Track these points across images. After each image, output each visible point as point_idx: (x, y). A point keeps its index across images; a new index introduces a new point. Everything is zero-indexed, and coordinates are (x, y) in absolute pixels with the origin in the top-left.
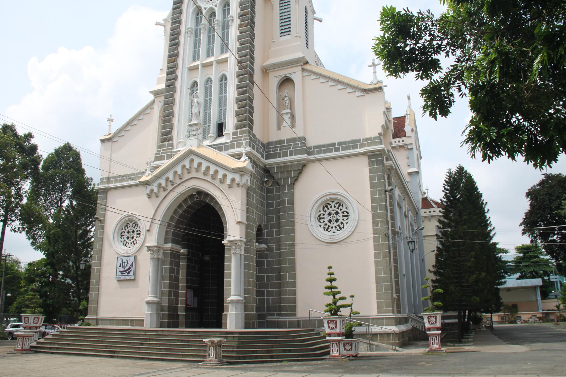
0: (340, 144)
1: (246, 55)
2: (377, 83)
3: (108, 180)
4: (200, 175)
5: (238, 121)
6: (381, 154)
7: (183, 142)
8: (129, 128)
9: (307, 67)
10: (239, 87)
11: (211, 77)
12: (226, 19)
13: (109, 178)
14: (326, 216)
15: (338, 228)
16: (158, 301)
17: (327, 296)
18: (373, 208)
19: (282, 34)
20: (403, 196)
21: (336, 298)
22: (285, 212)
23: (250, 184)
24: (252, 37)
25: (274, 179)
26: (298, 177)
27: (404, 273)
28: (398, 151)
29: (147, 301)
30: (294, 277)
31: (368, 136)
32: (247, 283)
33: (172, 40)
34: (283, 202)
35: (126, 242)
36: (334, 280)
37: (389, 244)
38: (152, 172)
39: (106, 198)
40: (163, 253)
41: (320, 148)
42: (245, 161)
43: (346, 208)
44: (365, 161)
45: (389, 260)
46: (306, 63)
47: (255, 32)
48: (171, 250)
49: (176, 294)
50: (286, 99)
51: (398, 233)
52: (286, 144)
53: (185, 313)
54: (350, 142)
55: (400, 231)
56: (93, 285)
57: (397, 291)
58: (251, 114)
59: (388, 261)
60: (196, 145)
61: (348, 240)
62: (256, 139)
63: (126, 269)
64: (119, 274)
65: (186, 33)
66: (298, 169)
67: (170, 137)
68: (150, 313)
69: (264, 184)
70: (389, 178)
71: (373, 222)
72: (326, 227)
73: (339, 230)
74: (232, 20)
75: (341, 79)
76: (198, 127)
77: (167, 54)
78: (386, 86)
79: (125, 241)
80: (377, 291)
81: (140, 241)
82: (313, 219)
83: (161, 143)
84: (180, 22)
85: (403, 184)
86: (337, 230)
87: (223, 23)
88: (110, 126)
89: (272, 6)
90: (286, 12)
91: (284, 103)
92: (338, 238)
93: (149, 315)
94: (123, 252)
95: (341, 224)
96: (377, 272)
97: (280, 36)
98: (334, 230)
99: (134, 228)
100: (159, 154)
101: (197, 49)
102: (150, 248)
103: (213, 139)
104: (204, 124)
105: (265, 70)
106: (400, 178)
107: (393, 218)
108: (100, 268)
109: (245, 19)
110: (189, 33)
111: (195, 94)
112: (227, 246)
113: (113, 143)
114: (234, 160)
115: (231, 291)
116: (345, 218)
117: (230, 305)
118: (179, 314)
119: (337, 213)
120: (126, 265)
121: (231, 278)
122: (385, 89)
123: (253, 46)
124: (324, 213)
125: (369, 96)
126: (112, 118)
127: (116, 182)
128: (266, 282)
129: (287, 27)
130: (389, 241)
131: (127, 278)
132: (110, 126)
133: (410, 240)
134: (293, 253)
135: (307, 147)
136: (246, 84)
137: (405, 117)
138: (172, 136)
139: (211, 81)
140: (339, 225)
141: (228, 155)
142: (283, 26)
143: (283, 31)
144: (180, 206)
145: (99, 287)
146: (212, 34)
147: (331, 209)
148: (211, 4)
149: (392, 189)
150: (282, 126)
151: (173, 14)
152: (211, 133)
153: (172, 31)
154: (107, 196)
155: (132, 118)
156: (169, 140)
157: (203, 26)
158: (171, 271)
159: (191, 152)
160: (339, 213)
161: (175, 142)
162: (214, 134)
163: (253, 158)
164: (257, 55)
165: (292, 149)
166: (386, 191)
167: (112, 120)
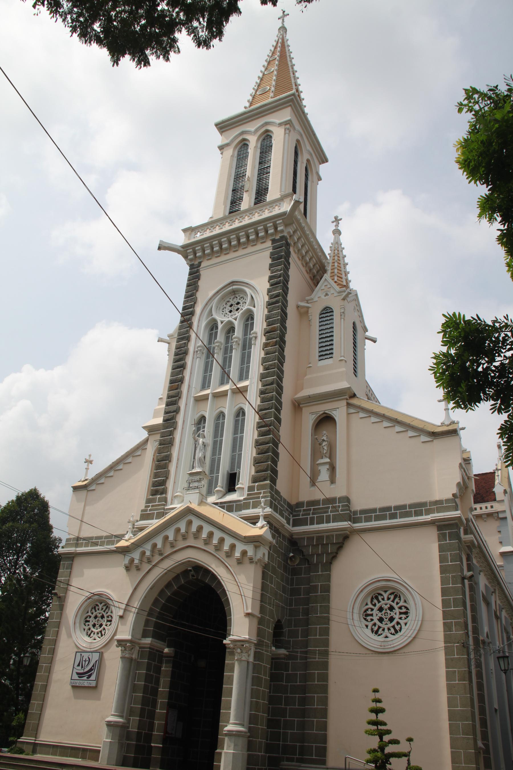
0: (397, 508)
1: (272, 383)
2: (450, 424)
3: (77, 541)
4: (200, 544)
5: (257, 472)
6: (456, 524)
7: (180, 496)
8: (111, 474)
9: (354, 401)
10: (259, 426)
11: (224, 411)
12: (248, 337)
13: (78, 539)
14: (375, 612)
15: (392, 631)
16: (124, 723)
17: (370, 736)
18: (445, 603)
19: (322, 358)
20: (492, 586)
21: (384, 740)
23: (269, 559)
24: (281, 359)
25: (303, 555)
26: (337, 553)
27: (496, 706)
28: (485, 521)
29: (107, 722)
30: (325, 701)
31: (437, 498)
32: (254, 706)
33: (175, 361)
34: (314, 589)
35: (90, 631)
36: (382, 711)
37: (469, 660)
38: (134, 535)
39: (71, 567)
40: (139, 651)
42: (262, 527)
43: (405, 601)
44: (433, 533)
45: (470, 684)
46: (352, 395)
47: (285, 353)
48: (150, 648)
49: (152, 715)
50: (324, 444)
51: (484, 642)
52: (321, 506)
53: (161, 746)
54: (411, 506)
55: (486, 640)
57: (485, 737)
58: (275, 462)
59: (468, 686)
60: (197, 502)
61: (406, 650)
62: (281, 497)
63: (86, 670)
64: (76, 677)
65: (196, 353)
66: (337, 542)
67: (164, 489)
68: (110, 740)
69: (289, 561)
70: (469, 559)
71: (444, 624)
72: (376, 628)
73: (394, 634)
74: (256, 338)
75: (400, 419)
76: (201, 477)
77: (169, 378)
78: (463, 429)
79: (89, 629)
80: (450, 734)
81: (109, 631)
82: (356, 616)
83: (151, 497)
84: (188, 339)
85: (491, 569)
86: (391, 634)
87: (244, 342)
88: (87, 469)
89: (310, 321)
90: (327, 329)
91: (322, 450)
92: (392, 646)
93: (109, 744)
94: (84, 645)
96: (451, 702)
97: (319, 360)
99: (104, 611)
100: (146, 511)
101: (208, 374)
102: (120, 643)
103: (221, 495)
104: (211, 474)
105: (297, 404)
106: (486, 560)
107: (474, 619)
108: (51, 666)
109: (273, 336)
110: (198, 352)
111: (201, 432)
112: (229, 648)
113: (90, 493)
114: (247, 524)
115: (229, 717)
116: (404, 616)
117: (226, 739)
118: (152, 746)
119: (391, 608)
120: (86, 665)
121: (231, 697)
122: (461, 433)
123: (282, 372)
125: (438, 443)
126: (91, 459)
127: (86, 545)
128: (283, 706)
129: (328, 348)
130: (468, 654)
131: (86, 684)
132: (87, 469)
133: (501, 654)
134: (325, 665)
135: (351, 511)
136: (270, 422)
137: (494, 473)
138: (167, 488)
139: (224, 416)
140: (393, 627)
141: (240, 518)
142: (323, 347)
143: (324, 353)
144: (169, 585)
145: (45, 694)
146: (228, 355)
147: (382, 602)
148: (229, 316)
149: (472, 576)
150: (318, 481)
151: (180, 328)
152: (219, 486)
153: (177, 349)
154: (72, 564)
155: (117, 460)
156: (162, 493)
157: (217, 344)
158: (148, 678)
159: (189, 511)
160: (395, 609)
161: (169, 496)
162: (222, 488)
163: (274, 524)
164: (287, 383)
165: (329, 513)
166: (463, 578)
167: (91, 462)
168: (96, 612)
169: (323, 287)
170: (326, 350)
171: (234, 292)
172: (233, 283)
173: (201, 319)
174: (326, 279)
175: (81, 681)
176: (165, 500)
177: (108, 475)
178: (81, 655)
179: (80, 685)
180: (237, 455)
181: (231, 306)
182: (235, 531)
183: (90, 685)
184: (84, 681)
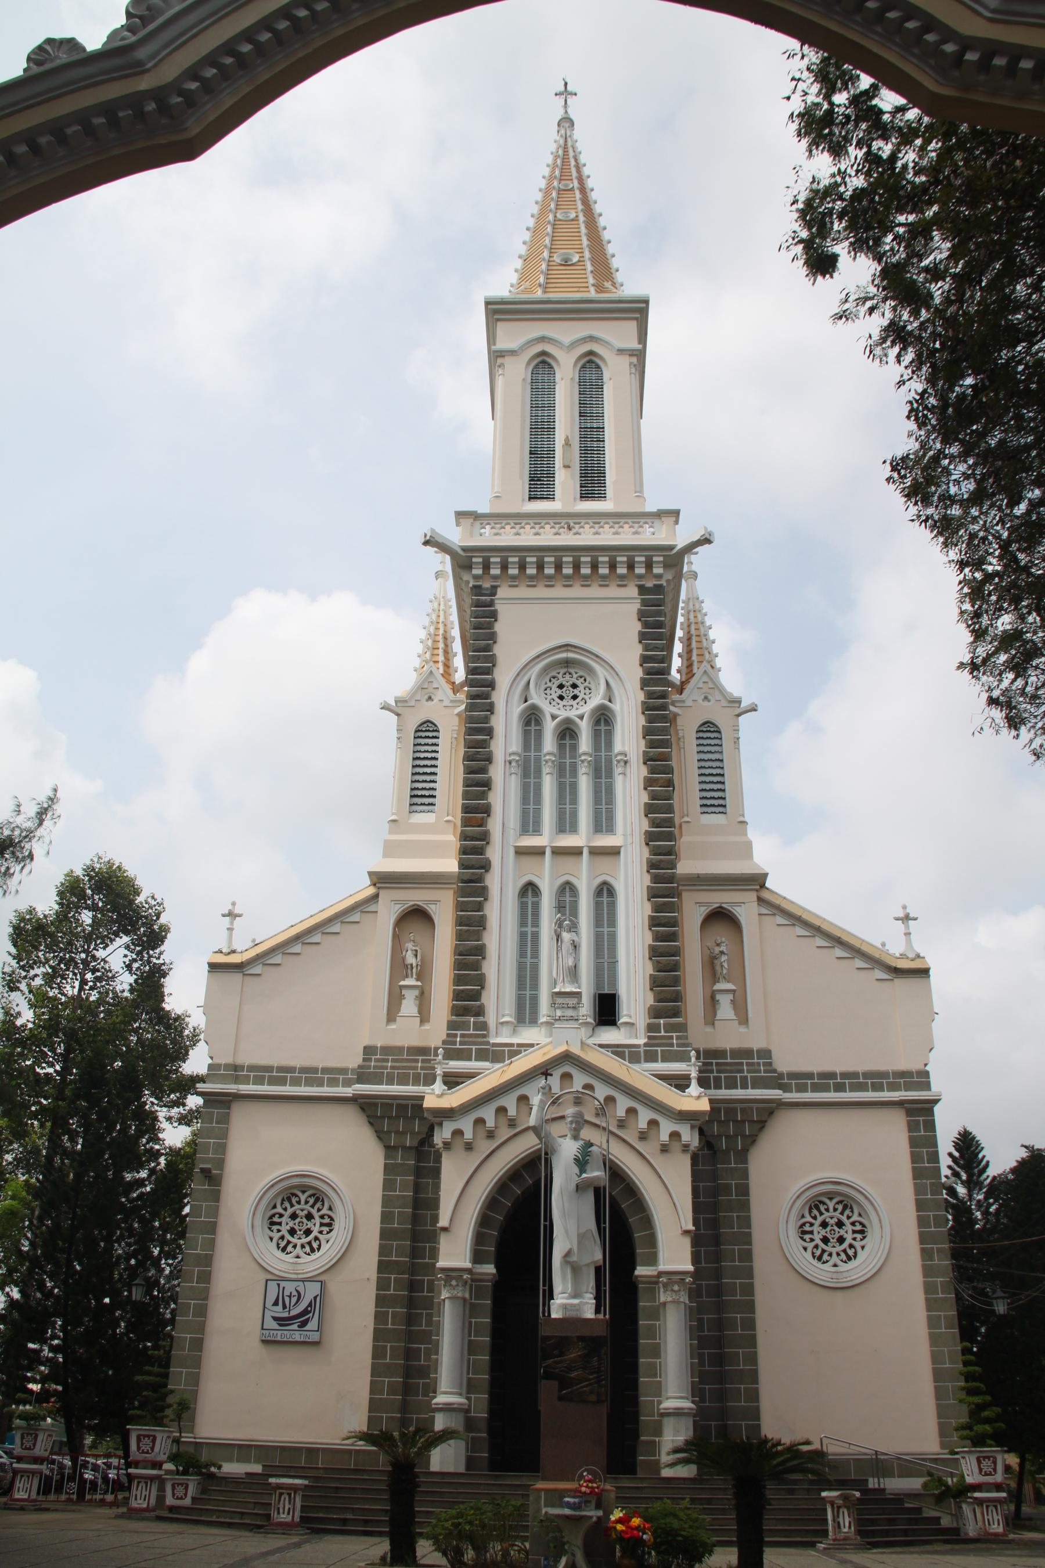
0: (845, 1075)
14: (816, 1228)
19: (705, 809)
22: (731, 1211)
35: (285, 1242)
41: (801, 1080)
43: (330, 1209)
50: (724, 958)
54: (867, 1075)
56: (183, 1349)
63: (293, 1313)
65: (508, 764)
71: (923, 1250)
72: (818, 1253)
75: (844, 938)
88: (230, 930)
92: (849, 1279)
95: (315, 1240)
98: (835, 1259)
116: (859, 1236)
119: (840, 1224)
120: (293, 1304)
124: (282, 1212)
125: (902, 985)
127: (259, 1081)
131: (297, 1337)
140: (845, 1251)
147: (826, 1214)
165: (745, 1074)
168: (294, 1208)
169: (701, 685)
170: (713, 798)
171: (567, 663)
172: (567, 647)
173: (509, 701)
174: (705, 671)
175: (285, 1332)
176: (484, 1026)
177: (289, 951)
178: (279, 1285)
179: (285, 1339)
180: (606, 964)
181: (561, 686)
182: (660, 1099)
183: (307, 1340)
184: (292, 1332)
